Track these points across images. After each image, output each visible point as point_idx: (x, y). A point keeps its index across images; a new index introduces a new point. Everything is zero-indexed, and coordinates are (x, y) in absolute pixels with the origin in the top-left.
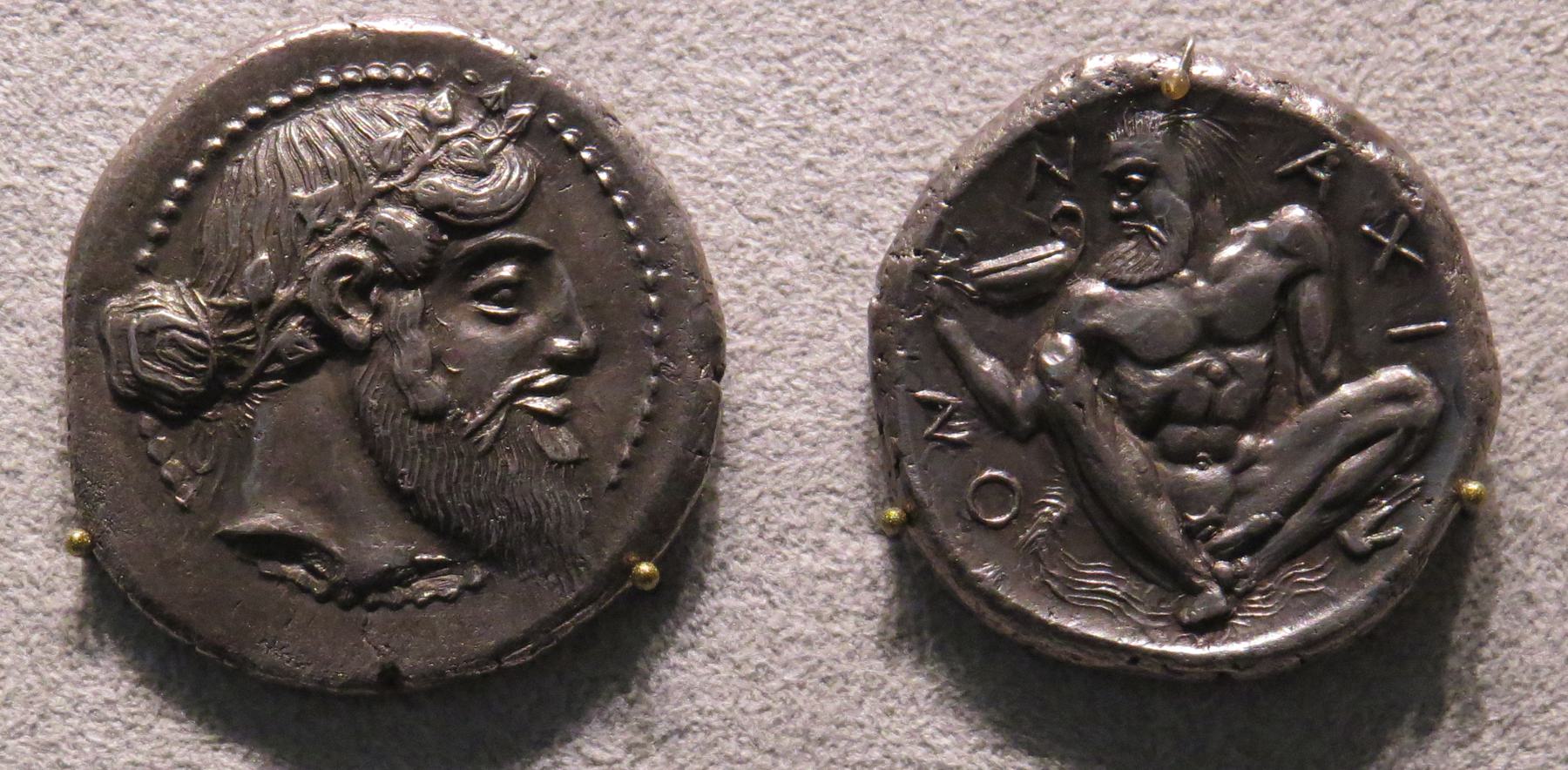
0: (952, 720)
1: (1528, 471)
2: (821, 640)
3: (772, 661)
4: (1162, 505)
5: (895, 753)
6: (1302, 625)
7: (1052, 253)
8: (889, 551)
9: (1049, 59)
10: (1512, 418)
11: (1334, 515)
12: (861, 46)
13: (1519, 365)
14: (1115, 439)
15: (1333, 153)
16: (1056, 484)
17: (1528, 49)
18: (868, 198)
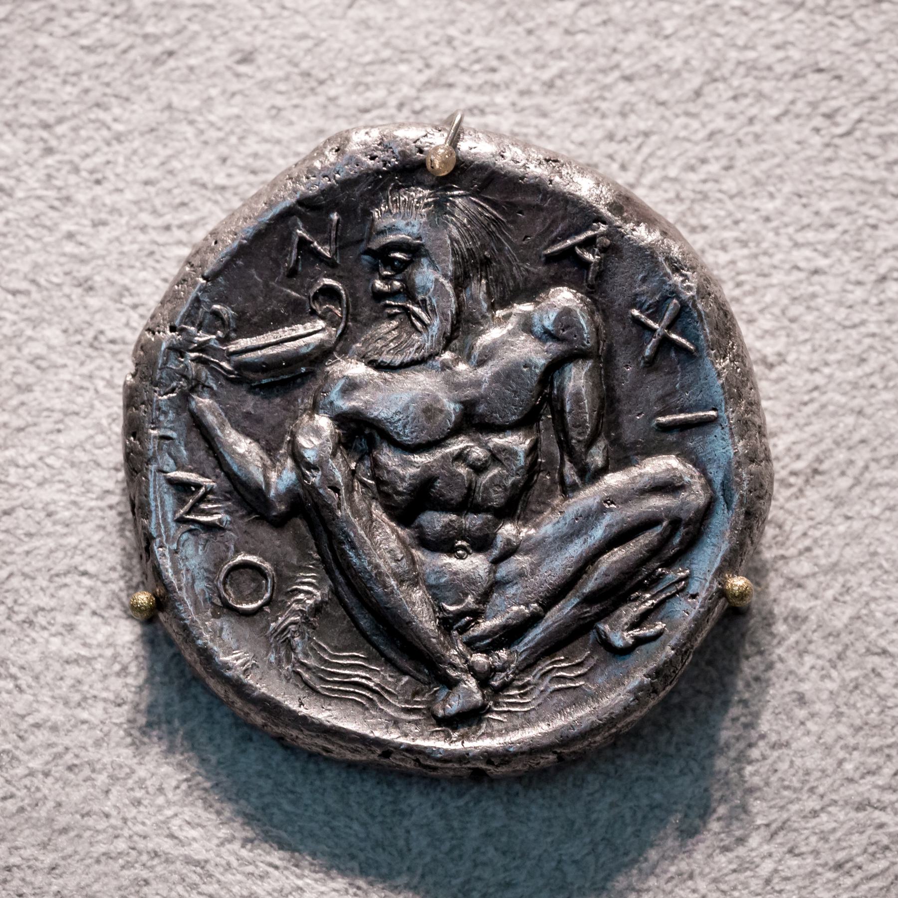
0: (200, 812)
1: (804, 567)
2: (68, 726)
3: (17, 748)
4: (418, 594)
5: (141, 844)
6: (559, 722)
7: (311, 333)
8: (143, 635)
9: (321, 132)
10: (790, 513)
11: (596, 608)
12: (127, 115)
13: (798, 457)
14: (370, 526)
15: (602, 235)
16: (311, 570)
17: (817, 130)
18: (130, 273)
